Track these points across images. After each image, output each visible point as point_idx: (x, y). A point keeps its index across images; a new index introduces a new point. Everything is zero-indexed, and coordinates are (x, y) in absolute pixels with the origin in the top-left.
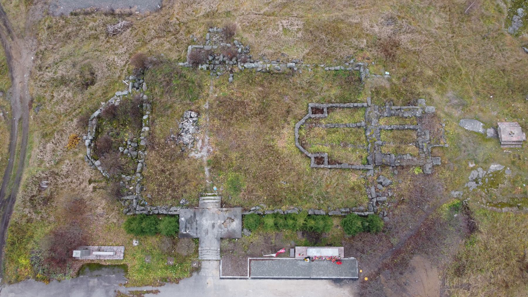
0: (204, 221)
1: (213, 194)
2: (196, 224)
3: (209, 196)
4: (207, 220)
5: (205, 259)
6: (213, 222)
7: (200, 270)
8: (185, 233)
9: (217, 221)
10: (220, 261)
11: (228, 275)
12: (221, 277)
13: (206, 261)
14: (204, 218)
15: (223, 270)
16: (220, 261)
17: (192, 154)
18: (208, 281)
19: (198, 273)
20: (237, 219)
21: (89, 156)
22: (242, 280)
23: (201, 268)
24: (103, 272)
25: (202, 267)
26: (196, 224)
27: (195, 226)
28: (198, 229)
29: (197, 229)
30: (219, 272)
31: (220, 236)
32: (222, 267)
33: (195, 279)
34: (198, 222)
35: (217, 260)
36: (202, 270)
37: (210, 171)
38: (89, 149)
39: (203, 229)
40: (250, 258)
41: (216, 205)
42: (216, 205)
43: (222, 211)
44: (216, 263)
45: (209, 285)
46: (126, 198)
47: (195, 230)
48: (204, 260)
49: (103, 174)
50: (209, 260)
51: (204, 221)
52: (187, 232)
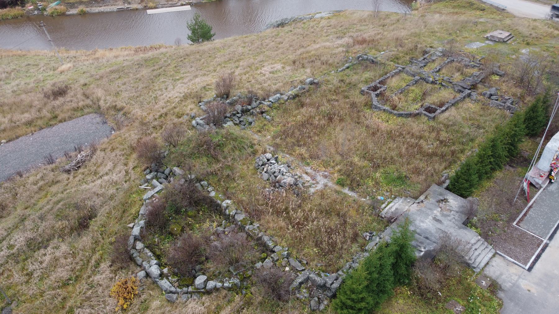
0: (422, 224)
1: (386, 203)
2: (419, 234)
3: (385, 207)
4: (423, 222)
5: (482, 265)
6: (430, 218)
7: (497, 283)
8: (422, 254)
9: (433, 213)
10: (496, 253)
11: (529, 258)
12: (527, 267)
13: (487, 269)
14: (417, 222)
15: (516, 258)
16: (496, 253)
17: (312, 190)
18: (523, 286)
19: (501, 289)
20: (447, 195)
21: (173, 289)
22: (544, 255)
23: (495, 281)
24: (490, 263)
25: (494, 277)
26: (419, 234)
27: (422, 237)
28: (430, 237)
29: (427, 238)
30: (516, 266)
31: (460, 224)
32: (511, 257)
33: (511, 300)
34: (418, 231)
35: (494, 256)
36: (500, 281)
37: (352, 189)
38: (165, 280)
39: (433, 232)
40: (515, 223)
41: (409, 202)
42: (409, 202)
43: (422, 202)
44: (497, 259)
45: (533, 290)
46: (296, 284)
47: (428, 241)
48: (483, 269)
49: (226, 285)
50: (488, 263)
51: (422, 224)
52: (423, 250)
